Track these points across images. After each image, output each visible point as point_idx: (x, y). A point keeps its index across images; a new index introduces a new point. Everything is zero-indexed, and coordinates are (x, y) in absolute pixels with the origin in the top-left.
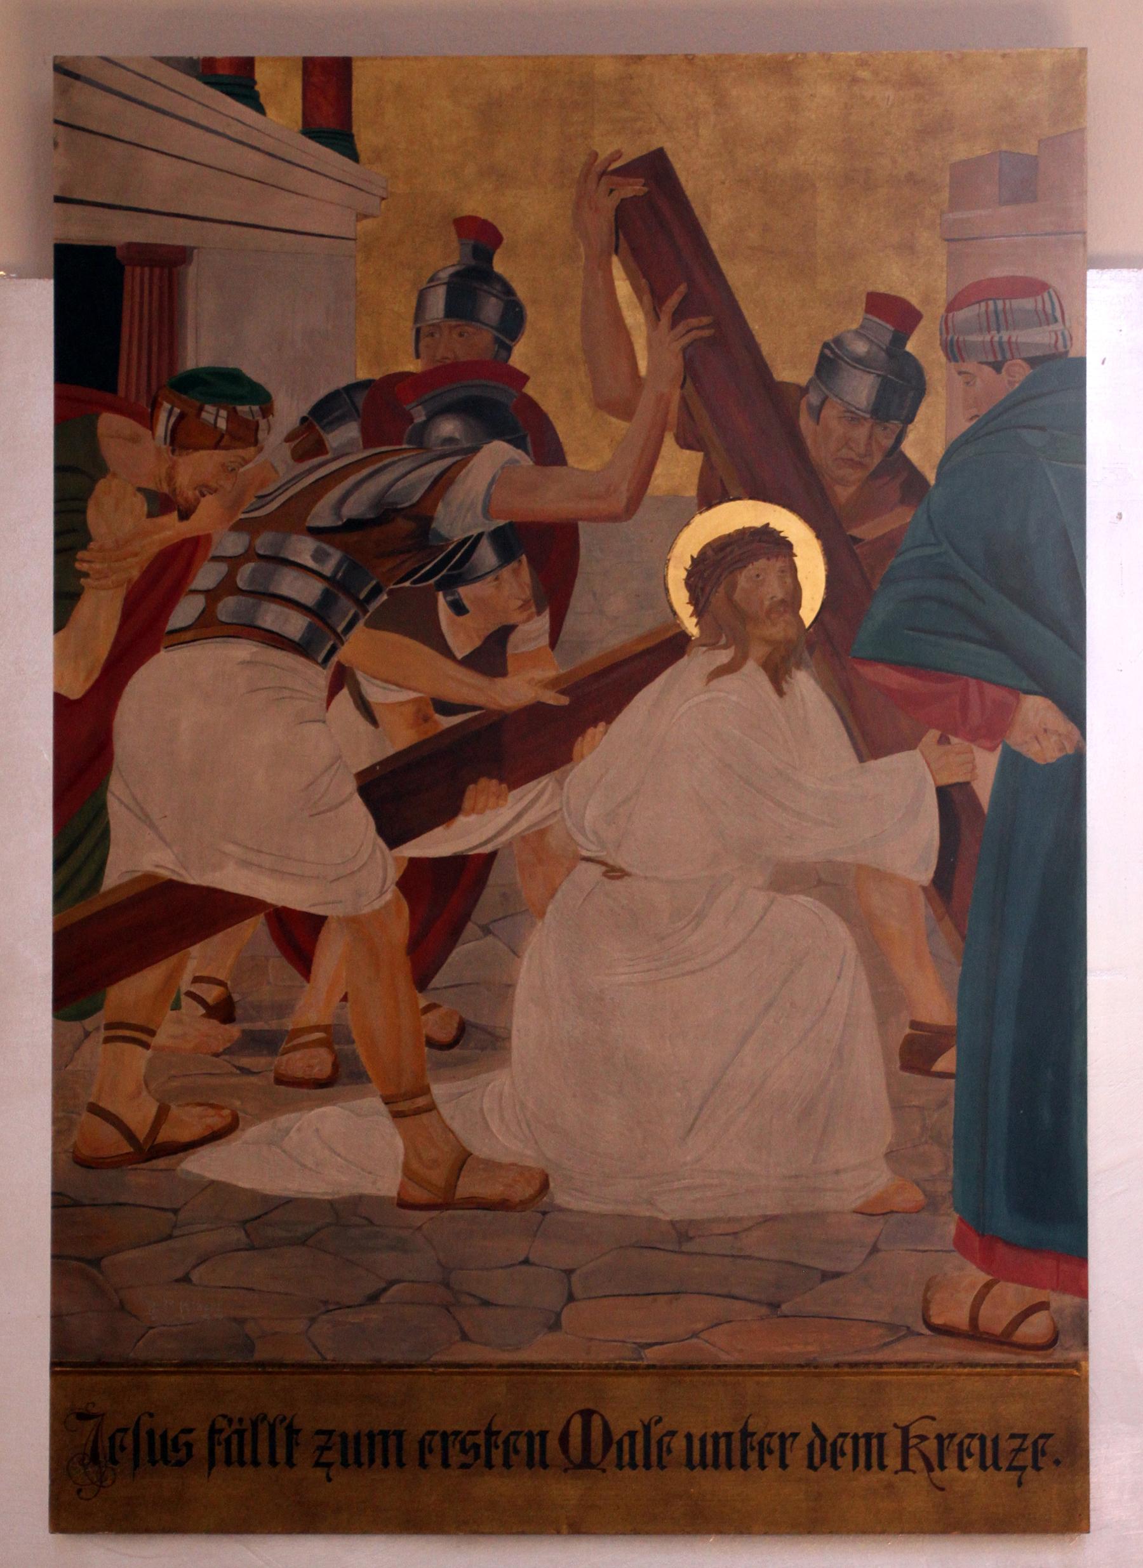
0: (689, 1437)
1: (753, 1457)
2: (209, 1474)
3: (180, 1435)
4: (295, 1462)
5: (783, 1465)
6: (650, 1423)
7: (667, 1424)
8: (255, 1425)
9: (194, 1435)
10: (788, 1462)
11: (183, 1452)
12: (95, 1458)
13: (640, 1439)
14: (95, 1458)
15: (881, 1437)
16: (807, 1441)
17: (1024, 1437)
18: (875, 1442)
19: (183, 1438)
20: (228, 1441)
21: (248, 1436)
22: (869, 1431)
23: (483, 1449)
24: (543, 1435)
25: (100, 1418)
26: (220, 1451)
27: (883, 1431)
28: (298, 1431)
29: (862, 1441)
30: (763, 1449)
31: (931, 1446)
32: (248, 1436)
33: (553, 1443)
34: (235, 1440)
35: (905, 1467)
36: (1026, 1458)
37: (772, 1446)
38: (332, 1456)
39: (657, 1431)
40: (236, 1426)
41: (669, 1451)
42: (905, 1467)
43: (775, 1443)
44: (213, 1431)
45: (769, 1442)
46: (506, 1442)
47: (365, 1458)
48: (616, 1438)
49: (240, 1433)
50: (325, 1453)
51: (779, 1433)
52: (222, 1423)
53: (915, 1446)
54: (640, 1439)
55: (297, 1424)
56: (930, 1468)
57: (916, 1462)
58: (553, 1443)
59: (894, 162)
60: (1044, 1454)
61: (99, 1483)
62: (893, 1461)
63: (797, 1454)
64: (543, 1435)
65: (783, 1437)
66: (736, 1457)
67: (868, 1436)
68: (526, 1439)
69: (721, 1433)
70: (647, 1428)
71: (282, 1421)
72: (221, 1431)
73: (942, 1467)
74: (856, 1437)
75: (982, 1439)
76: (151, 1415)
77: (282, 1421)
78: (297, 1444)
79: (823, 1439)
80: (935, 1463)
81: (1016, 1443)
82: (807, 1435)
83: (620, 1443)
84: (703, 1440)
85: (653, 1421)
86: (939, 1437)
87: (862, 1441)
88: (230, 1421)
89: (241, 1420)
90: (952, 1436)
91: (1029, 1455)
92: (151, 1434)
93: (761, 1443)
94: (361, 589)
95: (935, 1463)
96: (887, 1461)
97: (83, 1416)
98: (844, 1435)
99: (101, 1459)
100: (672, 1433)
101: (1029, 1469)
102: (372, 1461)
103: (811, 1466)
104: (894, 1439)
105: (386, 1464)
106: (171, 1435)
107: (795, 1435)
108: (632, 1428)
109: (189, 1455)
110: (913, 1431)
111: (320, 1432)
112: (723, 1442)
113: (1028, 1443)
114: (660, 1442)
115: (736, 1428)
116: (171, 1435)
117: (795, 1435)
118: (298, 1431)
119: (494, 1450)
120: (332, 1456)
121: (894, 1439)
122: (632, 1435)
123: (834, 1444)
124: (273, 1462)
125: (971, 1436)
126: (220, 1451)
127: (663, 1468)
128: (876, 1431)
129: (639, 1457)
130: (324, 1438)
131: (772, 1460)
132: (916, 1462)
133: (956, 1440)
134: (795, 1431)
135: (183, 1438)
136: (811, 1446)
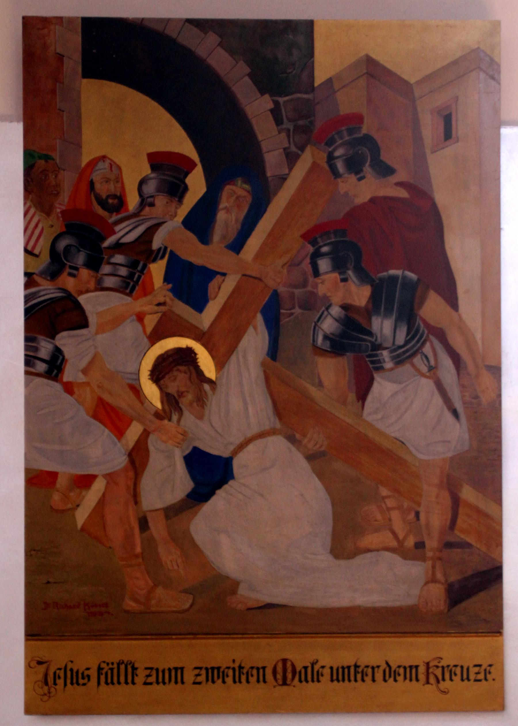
0: (331, 668)
3: (225, 670)
5: (374, 680)
7: (321, 663)
8: (119, 665)
9: (91, 670)
10: (376, 679)
11: (86, 681)
13: (309, 670)
15: (417, 667)
17: (480, 666)
18: (261, 671)
19: (86, 673)
20: (106, 674)
21: (115, 671)
22: (411, 664)
23: (80, 676)
24: (264, 668)
25: (48, 663)
26: (103, 678)
27: (265, 665)
28: (136, 669)
29: (210, 671)
30: (364, 674)
31: (439, 672)
32: (115, 671)
33: (269, 672)
34: (109, 672)
36: (481, 676)
38: (152, 679)
39: (316, 667)
40: (111, 666)
41: (322, 675)
42: (428, 682)
43: (370, 670)
44: (100, 669)
45: (367, 671)
48: (298, 670)
49: (112, 669)
51: (371, 666)
52: (103, 665)
54: (309, 670)
55: (136, 665)
56: (438, 681)
57: (432, 679)
58: (269, 672)
61: (48, 695)
62: (422, 677)
63: (379, 675)
64: (264, 668)
65: (373, 668)
66: (352, 678)
69: (171, 668)
70: (313, 664)
72: (103, 669)
73: (444, 680)
75: (405, 668)
76: (72, 662)
77: (130, 664)
78: (137, 675)
80: (440, 677)
81: (477, 669)
82: (384, 666)
83: (300, 672)
87: (210, 671)
88: (108, 664)
90: (448, 666)
92: (71, 670)
93: (362, 672)
94: (393, 269)
95: (440, 677)
97: (40, 663)
99: (50, 684)
100: (323, 667)
101: (155, 684)
102: (170, 681)
104: (422, 669)
107: (378, 667)
108: (305, 665)
109: (89, 680)
110: (431, 664)
112: (346, 671)
113: (483, 668)
118: (136, 669)
119: (242, 675)
120: (152, 679)
121: (422, 669)
122: (306, 668)
123: (395, 671)
125: (367, 667)
126: (103, 678)
127: (318, 681)
128: (216, 666)
129: (340, 677)
130: (149, 671)
131: (368, 679)
132: (432, 679)
133: (450, 668)
134: (378, 664)
136: (384, 671)
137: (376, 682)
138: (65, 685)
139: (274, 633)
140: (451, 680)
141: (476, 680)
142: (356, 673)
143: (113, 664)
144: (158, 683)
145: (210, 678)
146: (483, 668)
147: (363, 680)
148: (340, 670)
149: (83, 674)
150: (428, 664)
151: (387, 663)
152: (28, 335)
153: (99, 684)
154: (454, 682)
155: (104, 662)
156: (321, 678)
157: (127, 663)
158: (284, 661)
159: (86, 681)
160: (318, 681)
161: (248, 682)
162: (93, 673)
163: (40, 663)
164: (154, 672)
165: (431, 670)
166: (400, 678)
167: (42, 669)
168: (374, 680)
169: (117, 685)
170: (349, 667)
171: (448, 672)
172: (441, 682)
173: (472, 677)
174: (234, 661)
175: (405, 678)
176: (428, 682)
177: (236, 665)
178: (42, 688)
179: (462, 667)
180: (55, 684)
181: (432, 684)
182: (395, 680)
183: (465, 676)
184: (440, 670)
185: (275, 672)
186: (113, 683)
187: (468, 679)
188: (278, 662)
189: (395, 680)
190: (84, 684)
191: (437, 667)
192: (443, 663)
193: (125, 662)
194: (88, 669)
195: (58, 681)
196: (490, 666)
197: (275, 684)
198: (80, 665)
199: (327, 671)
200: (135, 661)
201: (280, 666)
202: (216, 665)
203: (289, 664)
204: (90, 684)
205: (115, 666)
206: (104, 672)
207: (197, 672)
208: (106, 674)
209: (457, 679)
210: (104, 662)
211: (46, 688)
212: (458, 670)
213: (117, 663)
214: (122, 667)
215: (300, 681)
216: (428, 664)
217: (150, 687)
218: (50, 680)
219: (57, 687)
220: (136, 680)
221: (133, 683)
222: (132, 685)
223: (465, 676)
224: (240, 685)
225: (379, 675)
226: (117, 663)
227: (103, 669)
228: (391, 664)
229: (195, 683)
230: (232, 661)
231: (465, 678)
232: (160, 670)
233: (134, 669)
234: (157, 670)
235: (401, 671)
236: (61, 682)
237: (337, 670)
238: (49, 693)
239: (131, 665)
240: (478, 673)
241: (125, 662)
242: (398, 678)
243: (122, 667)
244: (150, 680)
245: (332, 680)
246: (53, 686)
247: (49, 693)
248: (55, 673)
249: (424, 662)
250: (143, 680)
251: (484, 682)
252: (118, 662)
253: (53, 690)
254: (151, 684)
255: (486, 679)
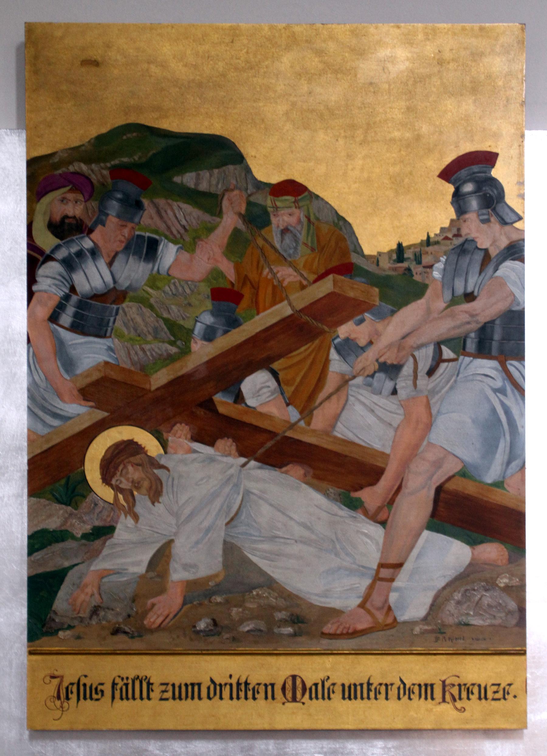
0: (343, 685)
1: (372, 694)
2: (77, 707)
4: (388, 698)
6: (324, 680)
11: (99, 696)
12: (59, 698)
14: (59, 698)
16: (397, 686)
17: (499, 685)
18: (269, 688)
19: (100, 687)
20: (121, 689)
26: (117, 694)
30: (377, 692)
31: (455, 691)
34: (124, 688)
35: (444, 700)
36: (500, 695)
37: (260, 690)
38: (169, 694)
39: (327, 685)
40: (125, 681)
41: (333, 692)
43: (383, 688)
44: (114, 684)
46: (376, 689)
47: (320, 696)
49: (127, 685)
50: (165, 694)
52: (118, 680)
53: (448, 691)
56: (454, 700)
57: (448, 697)
59: (14, 465)
60: (508, 693)
61: (61, 709)
63: (393, 692)
66: (365, 695)
67: (193, 685)
68: (264, 687)
69: (268, 684)
71: (145, 679)
72: (117, 684)
73: (460, 699)
74: (266, 685)
76: (86, 676)
77: (145, 679)
78: (152, 691)
79: (404, 685)
80: (457, 697)
81: (495, 688)
83: (311, 689)
84: (180, 687)
85: (325, 679)
86: (459, 685)
88: (122, 679)
89: (127, 678)
90: (465, 685)
91: (501, 692)
92: (85, 685)
95: (457, 697)
96: (435, 696)
97: (53, 677)
98: (414, 684)
100: (334, 684)
103: (399, 698)
105: (426, 698)
106: (94, 687)
107: (392, 684)
108: (317, 682)
110: (447, 682)
111: (162, 684)
114: (329, 689)
115: (365, 681)
116: (94, 687)
117: (392, 684)
118: (152, 684)
119: (240, 693)
122: (316, 685)
123: (409, 689)
124: (317, 698)
126: (117, 694)
127: (149, 698)
129: (130, 695)
135: (100, 687)
136: (399, 688)
137: (275, 701)
138: (78, 699)
139: (394, 649)
140: (468, 698)
141: (493, 699)
142: (369, 690)
143: (127, 678)
144: (174, 698)
145: (190, 694)
146: (502, 686)
147: (254, 698)
148: (352, 687)
149: (96, 689)
150: (444, 682)
151: (401, 680)
152: (523, 342)
153: (113, 698)
154: (379, 701)
155: (119, 677)
156: (332, 695)
157: (142, 678)
158: (294, 677)
159: (99, 696)
160: (329, 698)
161: (468, 698)
162: (107, 689)
163: (53, 677)
164: (170, 688)
165: (447, 689)
166: (415, 697)
167: (56, 682)
168: (387, 698)
169: (138, 701)
170: (361, 685)
171: (466, 690)
172: (458, 700)
173: (490, 695)
174: (231, 676)
175: (420, 696)
176: (444, 700)
177: (234, 681)
178: (54, 702)
179: (173, 685)
180: (68, 698)
181: (448, 703)
182: (410, 698)
183: (483, 695)
184: (457, 688)
185: (284, 688)
186: (127, 699)
187: (486, 698)
188: (287, 678)
189: (410, 698)
190: (97, 700)
191: (453, 685)
192: (462, 681)
193: (140, 678)
194: (102, 684)
195: (70, 696)
196: (510, 685)
197: (284, 700)
198: (91, 681)
199: (338, 689)
200: (151, 677)
201: (290, 683)
202: (196, 681)
203: (298, 682)
204: (103, 700)
205: (130, 681)
206: (119, 687)
207: (163, 688)
208: (121, 689)
209: (474, 697)
210: (119, 677)
211: (58, 703)
212: (476, 690)
213: (132, 679)
214: (137, 683)
215: (311, 698)
216: (444, 682)
217: (498, 702)
218: (63, 695)
219: (70, 702)
220: (152, 695)
221: (149, 698)
222: (361, 701)
223: (483, 695)
224: (349, 702)
225: (226, 692)
226: (132, 679)
227: (117, 684)
228: (405, 681)
229: (161, 699)
230: (228, 675)
231: (483, 695)
232: (483, 686)
233: (149, 684)
234: (479, 686)
235: (416, 688)
236: (74, 697)
237: (350, 687)
238: (62, 707)
239: (147, 680)
240: (495, 692)
241: (140, 678)
242: (412, 696)
243: (137, 683)
244: (166, 695)
245: (344, 698)
246: (65, 701)
247: (62, 707)
248: (67, 688)
249: (440, 680)
250: (159, 696)
251: (171, 701)
252: (133, 678)
253: (65, 705)
254: (167, 699)
255: (504, 698)
